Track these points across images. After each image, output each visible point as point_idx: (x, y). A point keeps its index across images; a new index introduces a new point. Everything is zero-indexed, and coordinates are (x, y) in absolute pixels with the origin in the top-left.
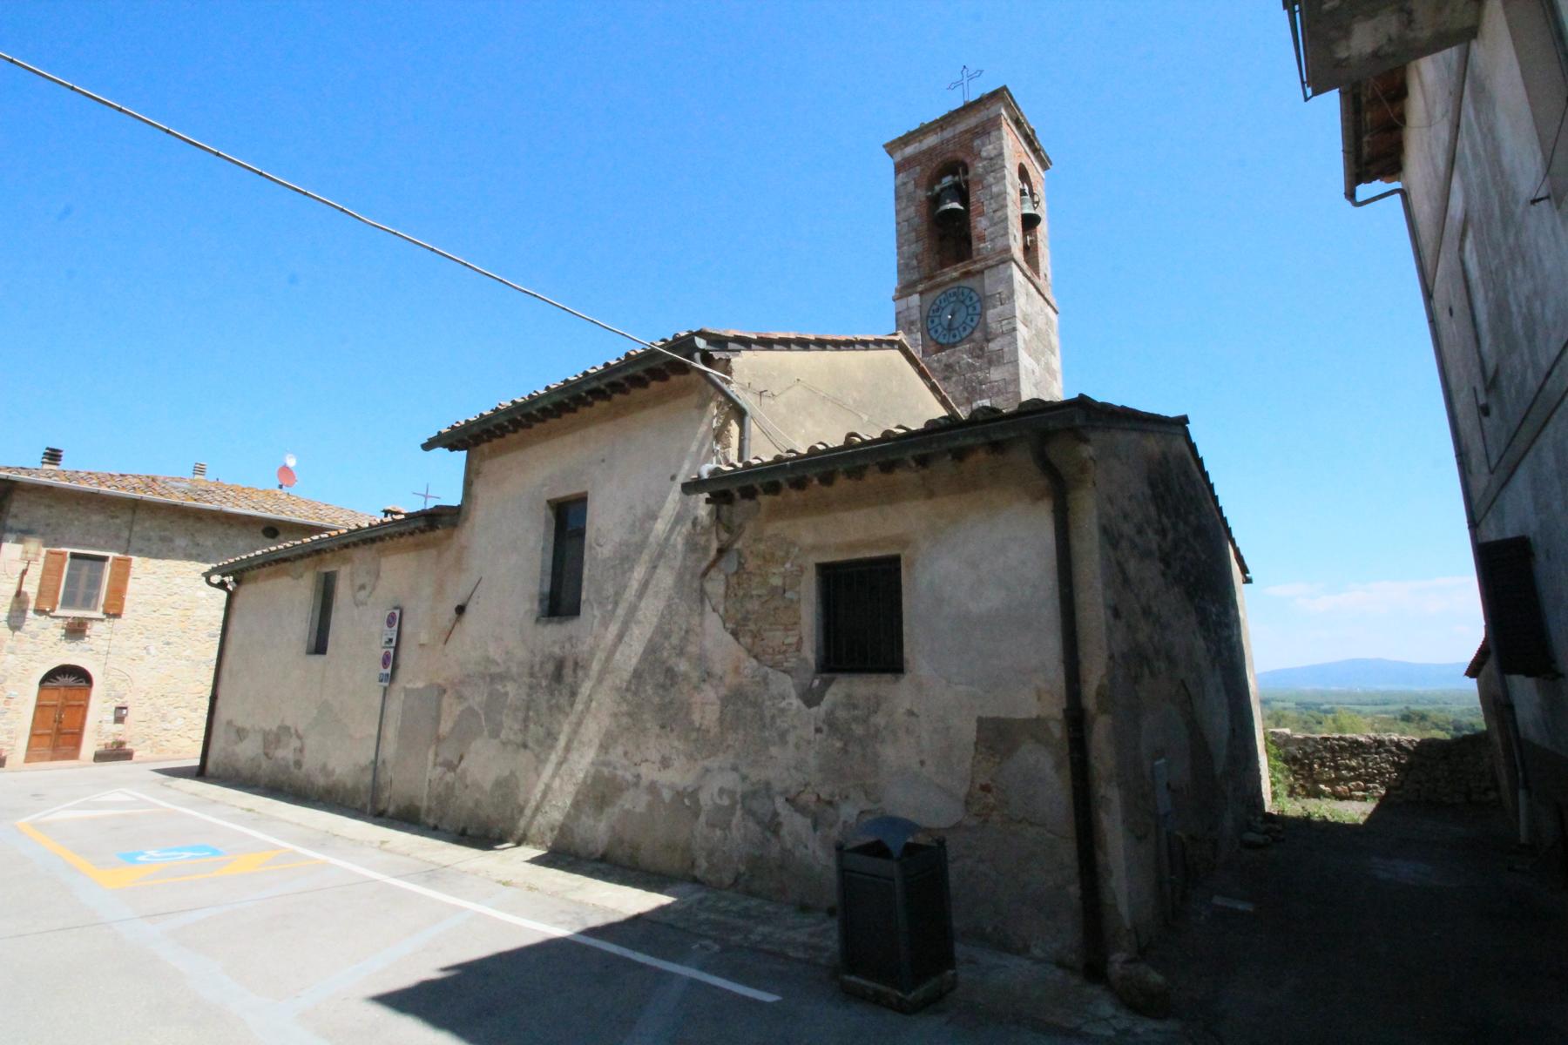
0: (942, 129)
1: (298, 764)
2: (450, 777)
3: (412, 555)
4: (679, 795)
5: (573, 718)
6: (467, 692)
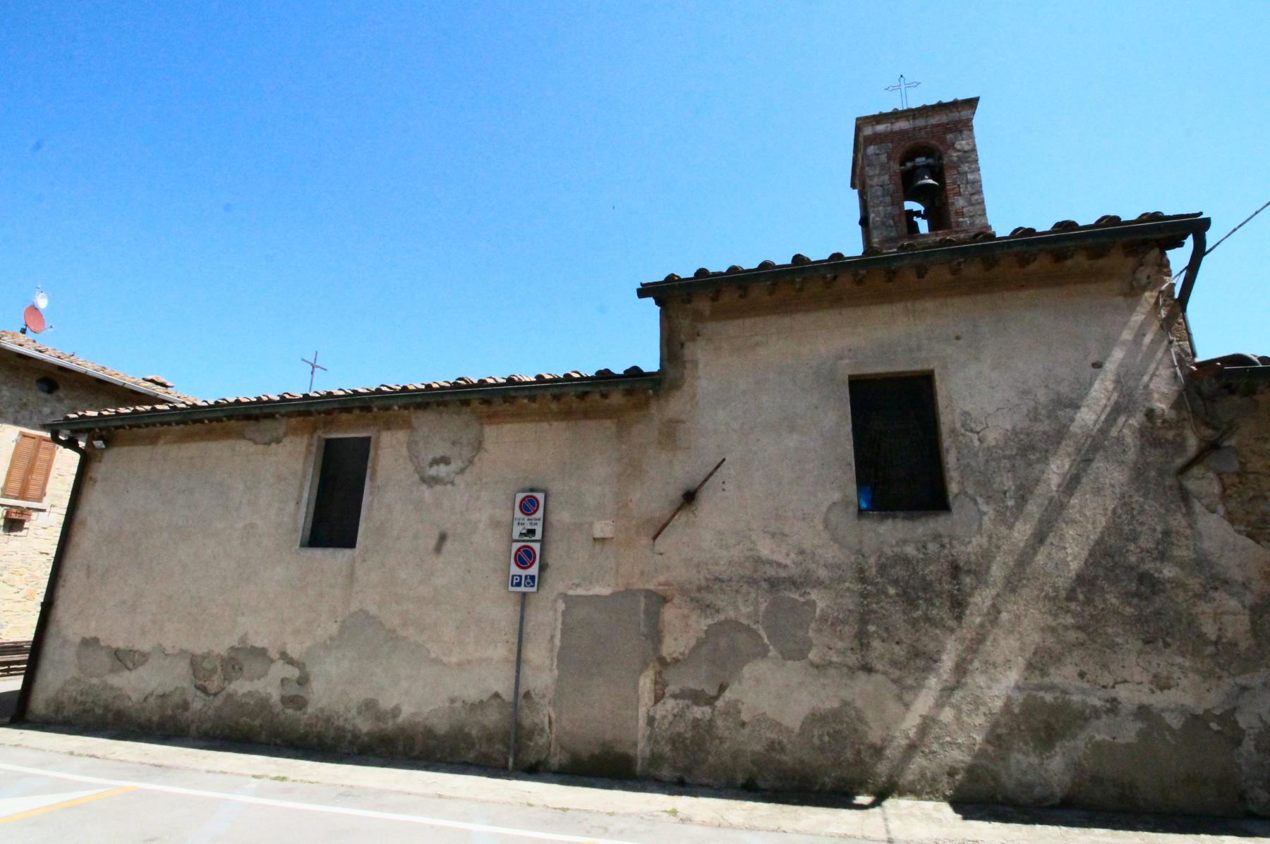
0: (914, 118)
1: (297, 702)
2: (700, 712)
3: (563, 425)
4: (1195, 721)
5: (966, 632)
6: (720, 600)
